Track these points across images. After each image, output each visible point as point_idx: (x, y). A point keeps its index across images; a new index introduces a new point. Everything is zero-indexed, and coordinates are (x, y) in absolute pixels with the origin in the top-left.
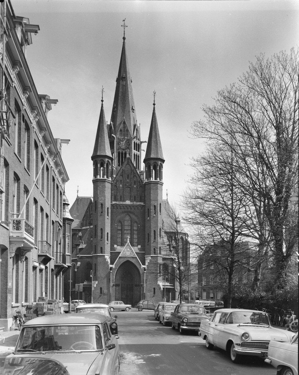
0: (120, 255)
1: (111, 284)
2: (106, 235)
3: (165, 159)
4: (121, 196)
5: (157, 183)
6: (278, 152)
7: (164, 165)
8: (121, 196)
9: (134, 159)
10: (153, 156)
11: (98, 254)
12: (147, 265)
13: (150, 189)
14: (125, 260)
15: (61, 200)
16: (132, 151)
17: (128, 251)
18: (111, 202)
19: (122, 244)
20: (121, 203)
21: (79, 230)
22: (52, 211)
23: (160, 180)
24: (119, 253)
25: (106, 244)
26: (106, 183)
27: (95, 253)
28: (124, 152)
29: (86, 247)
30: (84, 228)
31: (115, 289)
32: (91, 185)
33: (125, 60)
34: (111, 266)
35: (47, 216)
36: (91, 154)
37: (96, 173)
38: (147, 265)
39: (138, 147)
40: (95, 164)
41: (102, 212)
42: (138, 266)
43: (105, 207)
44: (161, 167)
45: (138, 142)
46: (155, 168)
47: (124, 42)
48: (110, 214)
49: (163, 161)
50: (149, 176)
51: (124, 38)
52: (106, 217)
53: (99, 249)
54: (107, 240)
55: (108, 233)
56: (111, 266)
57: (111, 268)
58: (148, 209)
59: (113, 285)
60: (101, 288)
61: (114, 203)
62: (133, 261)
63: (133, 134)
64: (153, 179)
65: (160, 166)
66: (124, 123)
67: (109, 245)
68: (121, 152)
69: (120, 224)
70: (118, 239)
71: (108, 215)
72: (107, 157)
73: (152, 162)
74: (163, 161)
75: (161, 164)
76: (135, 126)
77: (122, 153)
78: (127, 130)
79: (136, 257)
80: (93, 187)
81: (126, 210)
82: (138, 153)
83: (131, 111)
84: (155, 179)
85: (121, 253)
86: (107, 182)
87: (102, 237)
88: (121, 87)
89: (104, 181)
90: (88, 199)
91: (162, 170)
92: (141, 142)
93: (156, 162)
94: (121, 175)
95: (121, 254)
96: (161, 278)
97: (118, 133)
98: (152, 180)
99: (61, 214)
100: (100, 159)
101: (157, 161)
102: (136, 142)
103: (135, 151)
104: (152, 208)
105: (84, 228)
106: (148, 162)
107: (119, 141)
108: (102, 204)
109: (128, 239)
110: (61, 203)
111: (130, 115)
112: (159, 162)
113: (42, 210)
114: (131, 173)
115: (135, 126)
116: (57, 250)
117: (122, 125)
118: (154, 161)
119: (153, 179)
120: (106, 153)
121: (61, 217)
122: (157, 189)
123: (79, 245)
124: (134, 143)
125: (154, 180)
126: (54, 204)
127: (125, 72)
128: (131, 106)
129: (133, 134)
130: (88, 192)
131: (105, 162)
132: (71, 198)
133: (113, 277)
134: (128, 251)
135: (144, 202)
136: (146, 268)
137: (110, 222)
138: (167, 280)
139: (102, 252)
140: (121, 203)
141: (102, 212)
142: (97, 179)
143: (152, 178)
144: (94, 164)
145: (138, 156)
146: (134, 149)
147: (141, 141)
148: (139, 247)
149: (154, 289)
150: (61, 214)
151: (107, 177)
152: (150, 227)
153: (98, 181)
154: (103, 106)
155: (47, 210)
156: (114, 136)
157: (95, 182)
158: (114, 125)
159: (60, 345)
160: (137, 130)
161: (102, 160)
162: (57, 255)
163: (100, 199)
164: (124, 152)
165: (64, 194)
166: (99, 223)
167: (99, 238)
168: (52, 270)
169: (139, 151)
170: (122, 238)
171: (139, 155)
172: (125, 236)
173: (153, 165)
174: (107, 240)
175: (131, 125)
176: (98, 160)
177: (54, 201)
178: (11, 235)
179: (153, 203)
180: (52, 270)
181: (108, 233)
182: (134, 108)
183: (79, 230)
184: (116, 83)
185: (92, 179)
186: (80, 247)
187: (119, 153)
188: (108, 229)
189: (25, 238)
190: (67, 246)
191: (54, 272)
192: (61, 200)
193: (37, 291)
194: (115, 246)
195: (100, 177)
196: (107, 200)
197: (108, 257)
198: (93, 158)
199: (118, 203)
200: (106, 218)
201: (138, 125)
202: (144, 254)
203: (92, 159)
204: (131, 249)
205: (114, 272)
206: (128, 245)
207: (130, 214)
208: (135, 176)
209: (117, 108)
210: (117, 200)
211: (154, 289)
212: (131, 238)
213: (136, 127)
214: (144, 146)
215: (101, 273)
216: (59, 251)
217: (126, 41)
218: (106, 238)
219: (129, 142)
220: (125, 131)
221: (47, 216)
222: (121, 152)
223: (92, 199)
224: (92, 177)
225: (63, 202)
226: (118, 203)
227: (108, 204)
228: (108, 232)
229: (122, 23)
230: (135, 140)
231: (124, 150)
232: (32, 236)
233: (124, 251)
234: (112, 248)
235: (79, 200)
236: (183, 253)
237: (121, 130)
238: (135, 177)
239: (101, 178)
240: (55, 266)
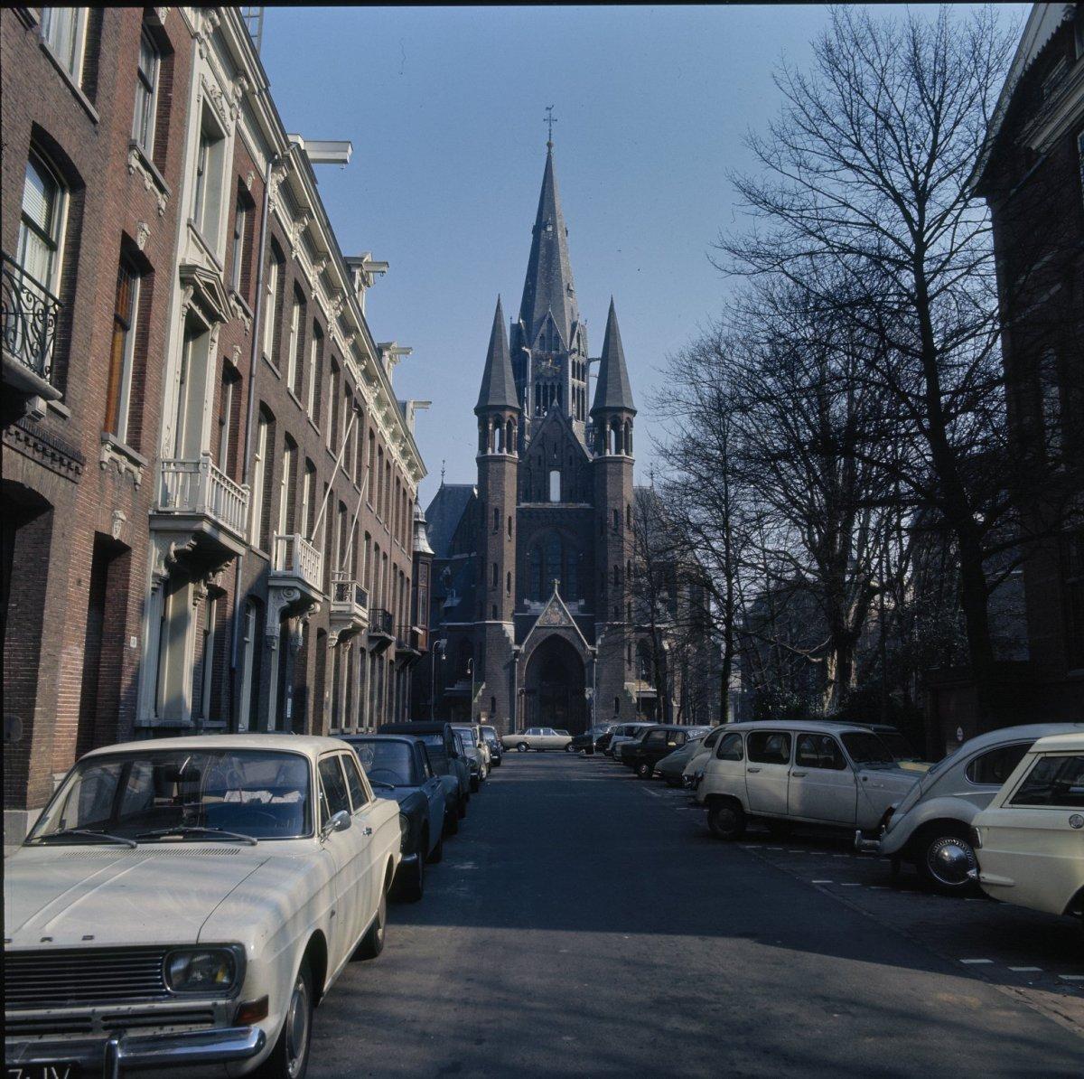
0: (537, 624)
1: (518, 690)
2: (505, 578)
4: (539, 491)
5: (620, 461)
6: (816, 442)
7: (636, 420)
8: (539, 491)
9: (573, 397)
10: (609, 403)
12: (599, 646)
13: (605, 473)
14: (548, 635)
15: (410, 515)
16: (567, 380)
17: (556, 614)
18: (518, 504)
19: (543, 597)
20: (540, 505)
21: (446, 563)
22: (393, 544)
23: (627, 454)
24: (535, 618)
25: (505, 597)
27: (483, 617)
28: (549, 384)
29: (459, 604)
30: (456, 557)
31: (526, 700)
33: (551, 188)
34: (516, 647)
35: (385, 557)
38: (599, 646)
39: (581, 371)
40: (483, 425)
41: (497, 528)
42: (577, 645)
43: (503, 516)
44: (629, 424)
45: (582, 360)
46: (615, 426)
47: (549, 152)
48: (514, 531)
49: (634, 412)
50: (600, 443)
51: (549, 145)
52: (507, 537)
53: (490, 609)
55: (509, 574)
56: (516, 647)
57: (517, 653)
59: (522, 692)
60: (493, 700)
61: (523, 505)
62: (567, 635)
64: (610, 453)
65: (626, 424)
66: (550, 321)
67: (513, 599)
68: (541, 384)
70: (533, 586)
71: (510, 534)
72: (505, 408)
73: (609, 415)
74: (634, 412)
76: (574, 325)
77: (545, 387)
78: (557, 338)
79: (574, 628)
83: (565, 294)
85: (540, 618)
87: (496, 582)
88: (542, 243)
89: (501, 460)
90: (469, 489)
92: (590, 361)
93: (615, 416)
94: (540, 445)
96: (631, 674)
97: (537, 344)
98: (608, 454)
99: (409, 543)
103: (576, 380)
104: (611, 516)
105: (456, 557)
107: (538, 360)
108: (497, 511)
110: (410, 521)
111: (562, 304)
112: (625, 415)
113: (377, 548)
114: (563, 437)
115: (574, 325)
116: (400, 621)
117: (544, 327)
119: (610, 453)
121: (409, 551)
122: (620, 473)
123: (444, 599)
124: (573, 362)
126: (397, 530)
128: (565, 284)
130: (466, 475)
132: (426, 493)
133: (520, 673)
134: (555, 613)
137: (514, 548)
138: (646, 678)
139: (495, 617)
140: (540, 505)
141: (497, 528)
143: (608, 451)
144: (479, 424)
145: (583, 392)
146: (573, 376)
147: (589, 357)
148: (582, 602)
149: (617, 700)
150: (409, 543)
151: (509, 451)
152: (605, 559)
155: (384, 547)
156: (527, 350)
157: (483, 462)
158: (528, 324)
162: (400, 630)
163: (492, 498)
164: (549, 384)
165: (416, 503)
166: (491, 552)
167: (490, 585)
168: (391, 662)
175: (564, 325)
176: (487, 413)
177: (397, 524)
178: (333, 608)
179: (611, 504)
180: (391, 662)
181: (509, 574)
182: (571, 288)
183: (446, 563)
186: (448, 604)
187: (538, 387)
188: (509, 565)
189: (356, 615)
190: (420, 605)
191: (396, 667)
192: (410, 515)
194: (526, 602)
195: (493, 451)
196: (507, 501)
197: (509, 628)
198: (478, 411)
200: (506, 541)
202: (593, 619)
204: (561, 608)
205: (524, 661)
206: (556, 600)
208: (571, 445)
209: (534, 289)
211: (617, 700)
214: (595, 368)
215: (496, 665)
216: (403, 624)
217: (553, 150)
218: (505, 584)
219: (561, 360)
220: (552, 340)
221: (385, 557)
223: (476, 492)
227: (510, 508)
228: (510, 569)
229: (546, 114)
230: (575, 356)
231: (549, 379)
232: (365, 607)
233: (546, 614)
234: (519, 606)
235: (446, 493)
237: (542, 337)
238: (571, 448)
239: (497, 453)
240: (397, 654)
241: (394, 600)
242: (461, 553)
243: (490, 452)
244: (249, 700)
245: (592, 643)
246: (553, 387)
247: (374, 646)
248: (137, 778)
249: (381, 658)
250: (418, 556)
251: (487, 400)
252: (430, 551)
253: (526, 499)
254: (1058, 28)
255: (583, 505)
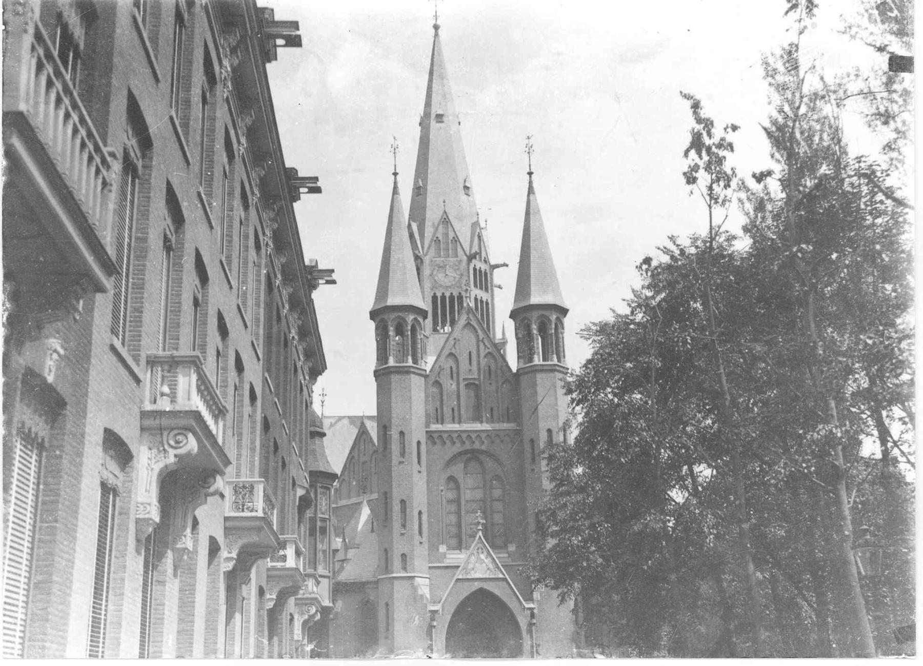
3: (566, 305)
11: (395, 575)
26: (412, 376)
32: (371, 385)
36: (369, 303)
37: (382, 356)
44: (559, 325)
45: (484, 267)
51: (436, 27)
54: (420, 533)
61: (434, 427)
68: (439, 295)
69: (452, 485)
73: (535, 315)
74: (564, 311)
75: (558, 318)
81: (468, 446)
82: (483, 295)
84: (544, 360)
86: (414, 373)
91: (562, 333)
100: (393, 316)
101: (547, 313)
106: (525, 315)
118: (541, 312)
120: (557, 291)
124: (475, 269)
125: (541, 362)
131: (550, 320)
136: (535, 611)
142: (388, 367)
145: (487, 304)
146: (476, 286)
147: (492, 263)
153: (391, 372)
154: (399, 185)
157: (382, 375)
160: (479, 237)
161: (399, 317)
169: (487, 290)
171: (489, 301)
173: (396, 323)
174: (420, 533)
184: (420, 128)
185: (373, 368)
199: (450, 427)
201: (482, 225)
203: (372, 318)
207: (478, 455)
210: (460, 418)
217: (440, 31)
222: (439, 295)
224: (371, 362)
253: (440, 420)
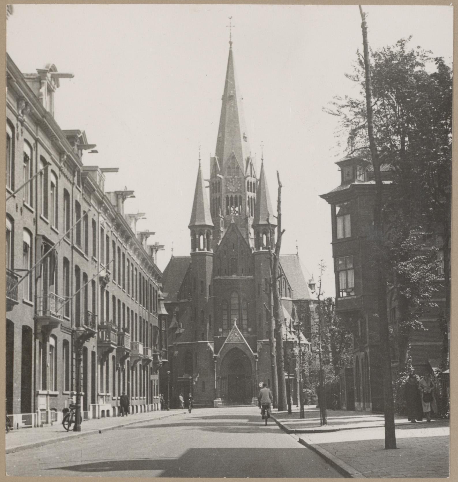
30: (182, 301)
34: (215, 355)
40: (193, 234)
42: (247, 353)
51: (231, 43)
57: (215, 358)
58: (259, 285)
63: (246, 172)
66: (233, 158)
68: (230, 196)
77: (232, 197)
78: (238, 168)
79: (245, 343)
80: (235, 5)
89: (204, 255)
95: (226, 340)
102: (250, 181)
105: (182, 301)
109: (235, 322)
127: (233, 87)
129: (246, 172)
135: (253, 274)
144: (191, 235)
151: (208, 250)
158: (221, 161)
159: (90, 142)
170: (228, 320)
172: (232, 316)
182: (245, 136)
186: (177, 332)
193: (59, 203)
199: (222, 278)
202: (256, 339)
212: (239, 320)
213: (250, 161)
217: (233, 45)
222: (230, 196)
225: (158, 298)
226: (222, 278)
236: (281, 353)
241: (147, 302)
242: (185, 298)
243: (197, 251)
244: (431, 435)
245: (255, 351)
246: (236, 197)
247: (145, 363)
248: (315, 360)
249: (147, 367)
250: (161, 316)
251: (195, 222)
252: (167, 313)
254: (329, 203)
255: (249, 277)
